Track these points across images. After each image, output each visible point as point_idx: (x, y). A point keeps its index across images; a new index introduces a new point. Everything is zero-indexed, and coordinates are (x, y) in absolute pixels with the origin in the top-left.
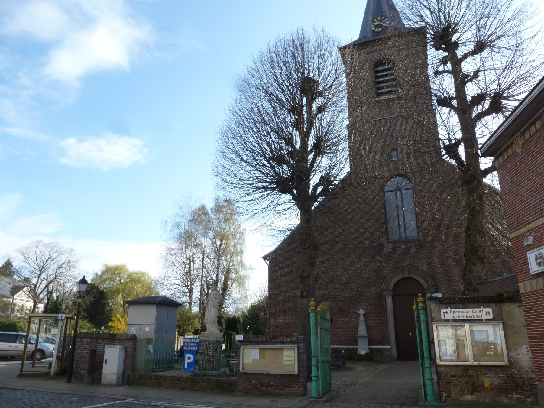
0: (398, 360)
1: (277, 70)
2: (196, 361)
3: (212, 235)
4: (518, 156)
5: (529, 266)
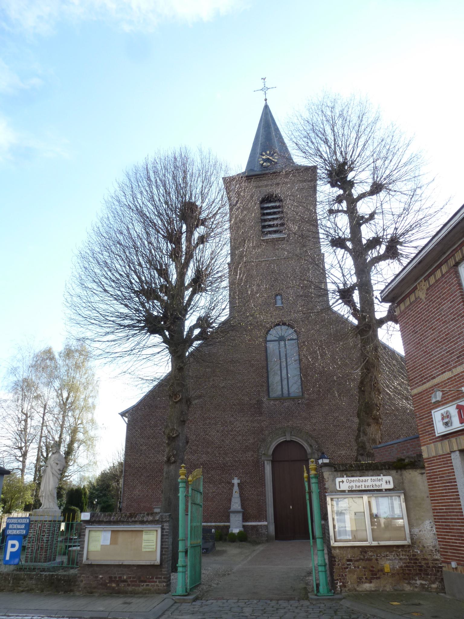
0: (276, 539)
1: (155, 190)
2: (23, 548)
3: (59, 385)
4: (421, 302)
5: (434, 427)
